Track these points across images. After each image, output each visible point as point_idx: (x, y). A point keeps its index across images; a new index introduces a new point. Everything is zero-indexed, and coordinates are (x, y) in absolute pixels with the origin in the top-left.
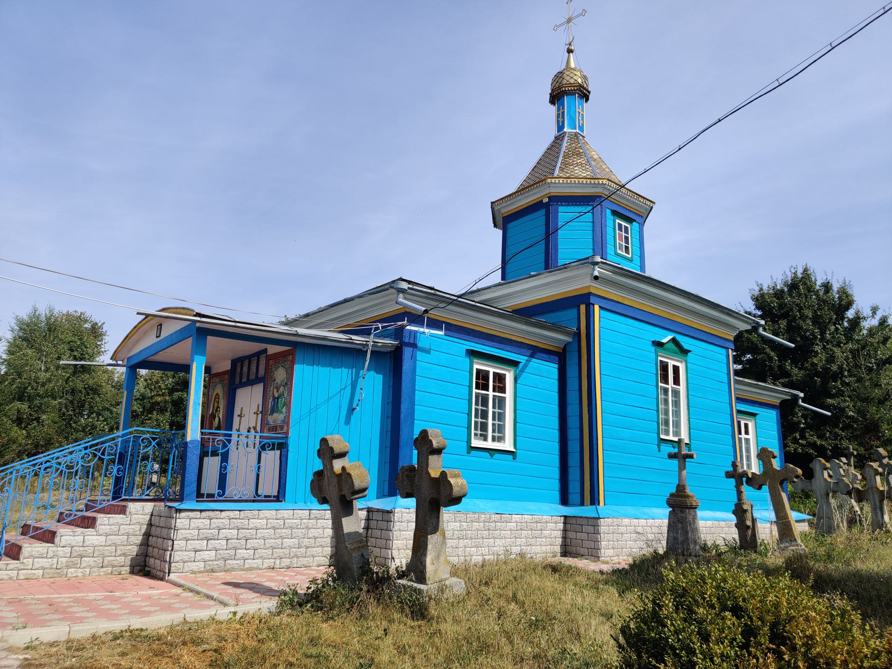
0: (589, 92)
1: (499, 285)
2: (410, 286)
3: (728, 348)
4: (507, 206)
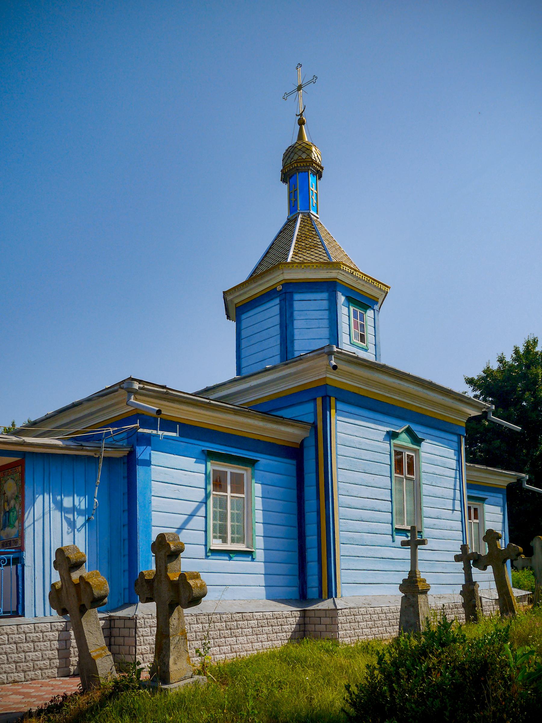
0: (322, 168)
1: (234, 381)
2: (141, 386)
3: (460, 435)
4: (240, 295)
